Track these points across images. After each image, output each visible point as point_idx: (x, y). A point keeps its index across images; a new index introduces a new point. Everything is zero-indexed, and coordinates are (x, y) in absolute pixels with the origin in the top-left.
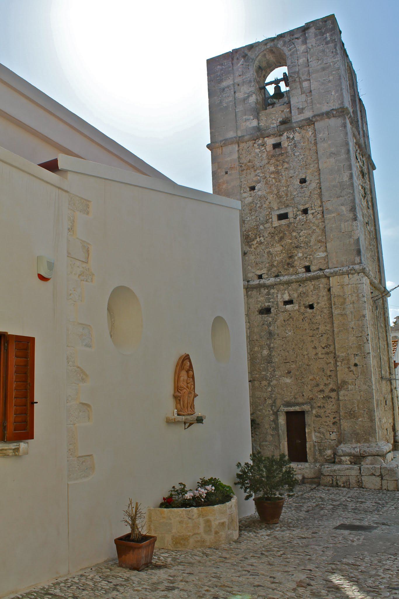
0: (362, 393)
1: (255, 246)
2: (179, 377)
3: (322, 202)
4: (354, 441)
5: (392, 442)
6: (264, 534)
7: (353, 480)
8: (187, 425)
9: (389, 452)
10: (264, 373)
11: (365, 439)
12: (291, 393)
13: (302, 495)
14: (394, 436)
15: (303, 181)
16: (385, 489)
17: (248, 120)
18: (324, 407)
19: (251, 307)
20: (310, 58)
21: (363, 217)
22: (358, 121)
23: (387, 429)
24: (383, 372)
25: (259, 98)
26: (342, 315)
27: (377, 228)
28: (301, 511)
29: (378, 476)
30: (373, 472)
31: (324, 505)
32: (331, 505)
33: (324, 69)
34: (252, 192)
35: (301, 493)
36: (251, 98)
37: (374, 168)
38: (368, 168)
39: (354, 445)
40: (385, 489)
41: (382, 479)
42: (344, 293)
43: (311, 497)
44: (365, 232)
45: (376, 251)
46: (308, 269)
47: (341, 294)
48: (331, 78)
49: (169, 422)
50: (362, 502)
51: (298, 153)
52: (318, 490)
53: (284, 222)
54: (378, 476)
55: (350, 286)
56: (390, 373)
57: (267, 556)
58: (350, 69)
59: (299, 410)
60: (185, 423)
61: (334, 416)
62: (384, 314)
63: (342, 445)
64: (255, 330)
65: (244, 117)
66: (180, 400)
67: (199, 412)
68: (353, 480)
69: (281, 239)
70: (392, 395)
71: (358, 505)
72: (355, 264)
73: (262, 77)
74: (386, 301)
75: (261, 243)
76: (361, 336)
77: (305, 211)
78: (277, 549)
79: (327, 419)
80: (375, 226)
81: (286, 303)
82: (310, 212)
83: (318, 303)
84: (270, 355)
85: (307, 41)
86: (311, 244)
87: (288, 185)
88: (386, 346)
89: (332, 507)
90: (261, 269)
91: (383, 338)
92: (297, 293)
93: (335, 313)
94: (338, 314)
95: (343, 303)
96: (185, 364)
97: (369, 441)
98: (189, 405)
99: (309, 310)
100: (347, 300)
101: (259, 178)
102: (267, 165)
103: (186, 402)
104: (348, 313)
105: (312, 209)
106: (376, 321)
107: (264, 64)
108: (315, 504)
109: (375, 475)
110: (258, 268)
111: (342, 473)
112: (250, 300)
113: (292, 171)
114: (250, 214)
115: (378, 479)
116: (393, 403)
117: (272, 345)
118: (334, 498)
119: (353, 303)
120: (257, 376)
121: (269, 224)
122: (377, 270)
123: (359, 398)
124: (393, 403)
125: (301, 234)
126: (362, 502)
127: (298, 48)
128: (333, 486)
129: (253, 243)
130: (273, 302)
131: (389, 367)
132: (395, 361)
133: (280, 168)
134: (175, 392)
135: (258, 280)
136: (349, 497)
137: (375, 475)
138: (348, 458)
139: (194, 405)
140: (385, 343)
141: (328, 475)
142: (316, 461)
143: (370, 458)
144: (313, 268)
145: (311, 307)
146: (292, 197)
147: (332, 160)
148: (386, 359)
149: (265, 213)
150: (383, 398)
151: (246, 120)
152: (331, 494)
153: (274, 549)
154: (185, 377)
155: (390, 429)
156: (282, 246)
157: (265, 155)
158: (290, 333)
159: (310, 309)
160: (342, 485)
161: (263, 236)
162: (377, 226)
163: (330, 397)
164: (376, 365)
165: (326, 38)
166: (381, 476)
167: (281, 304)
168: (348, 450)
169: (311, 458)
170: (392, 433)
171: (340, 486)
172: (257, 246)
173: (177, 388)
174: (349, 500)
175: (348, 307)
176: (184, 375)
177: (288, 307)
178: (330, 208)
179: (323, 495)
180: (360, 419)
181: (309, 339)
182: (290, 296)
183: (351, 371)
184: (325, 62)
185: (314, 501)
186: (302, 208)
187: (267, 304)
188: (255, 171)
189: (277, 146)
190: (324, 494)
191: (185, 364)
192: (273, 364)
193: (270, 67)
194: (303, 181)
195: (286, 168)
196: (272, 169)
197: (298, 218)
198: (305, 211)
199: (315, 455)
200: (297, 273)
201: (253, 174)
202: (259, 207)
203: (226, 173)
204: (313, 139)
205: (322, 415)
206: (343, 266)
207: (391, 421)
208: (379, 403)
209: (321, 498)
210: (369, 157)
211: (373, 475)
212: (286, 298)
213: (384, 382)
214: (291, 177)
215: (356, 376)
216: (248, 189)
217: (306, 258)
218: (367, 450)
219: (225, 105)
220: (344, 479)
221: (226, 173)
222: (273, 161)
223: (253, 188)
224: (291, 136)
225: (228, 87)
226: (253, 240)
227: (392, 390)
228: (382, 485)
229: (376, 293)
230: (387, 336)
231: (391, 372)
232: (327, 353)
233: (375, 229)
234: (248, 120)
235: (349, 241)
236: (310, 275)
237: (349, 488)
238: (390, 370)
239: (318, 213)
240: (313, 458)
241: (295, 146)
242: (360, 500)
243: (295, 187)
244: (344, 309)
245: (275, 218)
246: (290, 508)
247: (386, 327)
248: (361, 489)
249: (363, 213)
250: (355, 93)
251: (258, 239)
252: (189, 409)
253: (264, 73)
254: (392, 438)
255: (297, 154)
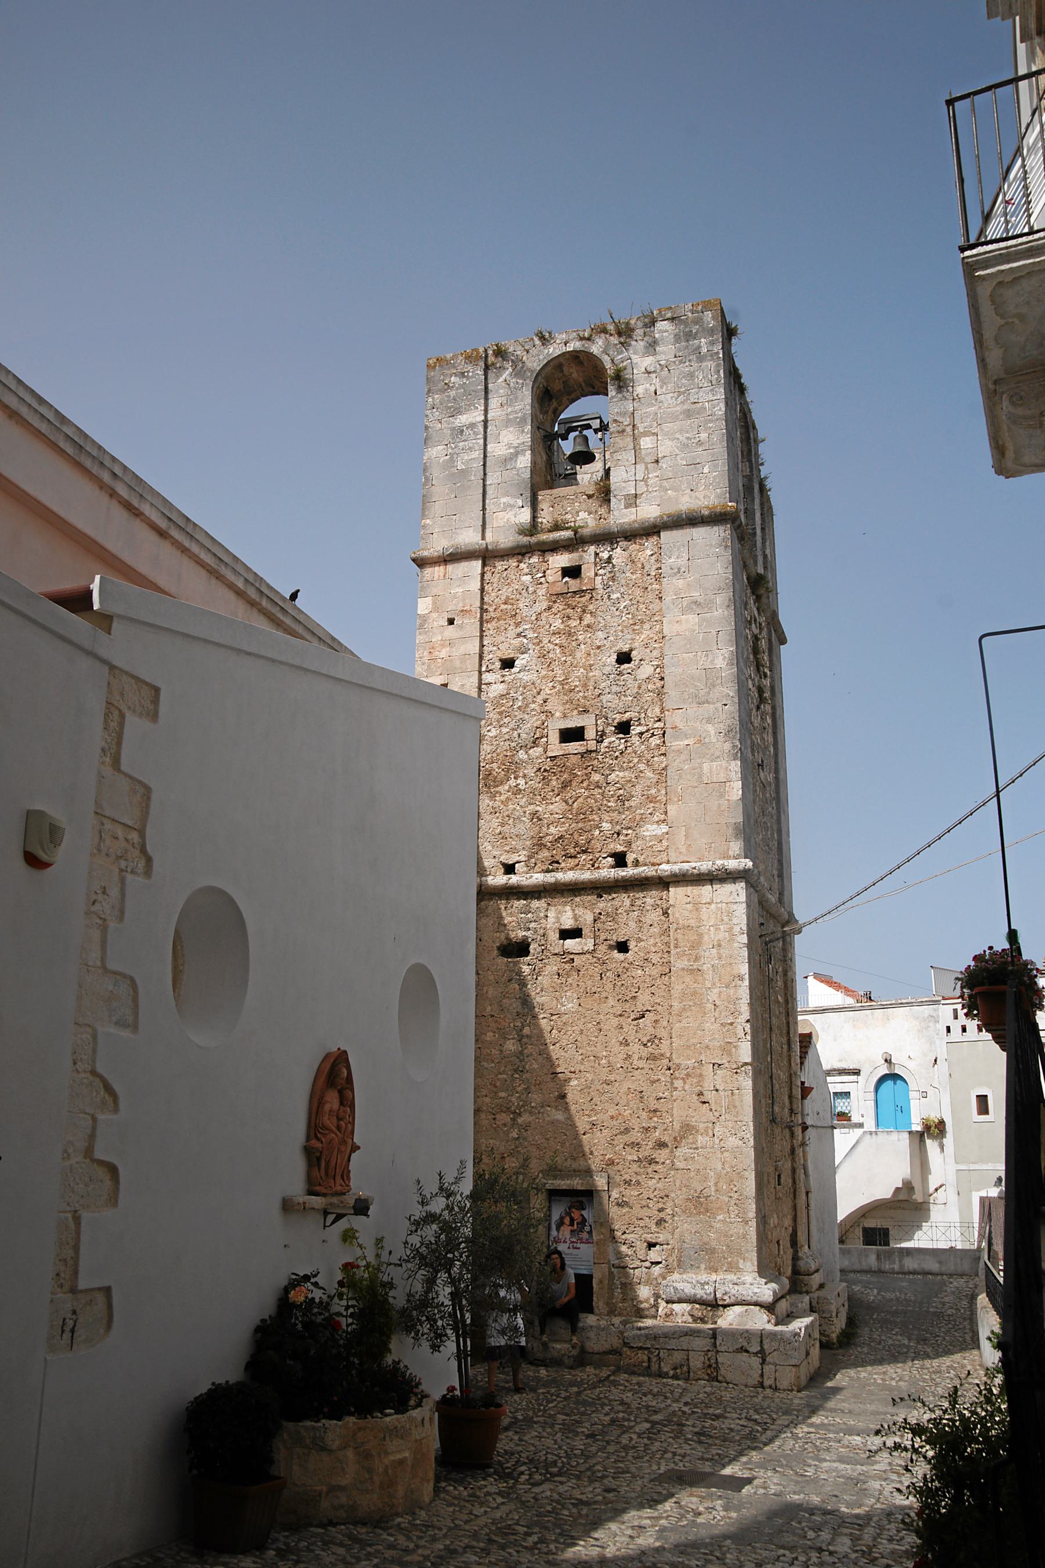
0: (726, 1154)
1: (503, 798)
2: (321, 1103)
3: (662, 711)
4: (703, 1266)
5: (789, 1272)
6: (493, 1489)
7: (697, 1362)
8: (331, 1218)
9: (782, 1297)
10: (502, 1094)
11: (730, 1263)
12: (563, 1144)
13: (579, 1393)
14: (793, 1259)
15: (624, 658)
16: (770, 1387)
17: (512, 506)
18: (638, 1183)
19: (485, 937)
20: (662, 387)
21: (753, 751)
22: (755, 534)
23: (778, 1242)
24: (776, 1109)
25: (539, 461)
26: (691, 971)
27: (781, 777)
28: (577, 1434)
29: (756, 1354)
30: (745, 1344)
31: (629, 1420)
32: (647, 1421)
33: (688, 414)
34: (506, 672)
35: (575, 1389)
36: (521, 458)
37: (783, 641)
38: (770, 641)
39: (704, 1277)
40: (770, 1387)
41: (764, 1362)
42: (699, 920)
43: (600, 1399)
44: (754, 785)
45: (775, 827)
46: (620, 860)
47: (692, 923)
48: (704, 436)
49: (287, 1206)
50: (717, 1417)
51: (619, 595)
52: (615, 1384)
53: (574, 747)
54: (756, 1354)
55: (713, 906)
56: (791, 1111)
57: (503, 1547)
58: (746, 418)
59: (580, 1188)
60: (326, 1213)
61: (661, 1205)
62: (785, 973)
63: (676, 1276)
64: (490, 993)
65: (504, 500)
66: (319, 1159)
67: (359, 1186)
68: (697, 1362)
69: (565, 785)
70: (793, 1160)
71: (707, 1425)
72: (729, 858)
73: (550, 412)
74: (791, 944)
75: (517, 791)
76: (731, 1024)
77: (624, 728)
78: (525, 1529)
79: (645, 1212)
80: (777, 771)
81: (566, 934)
82: (635, 730)
83: (639, 940)
84: (521, 1052)
85: (657, 349)
86: (632, 804)
87: (591, 665)
88: (785, 1047)
89: (648, 1425)
90: (514, 850)
91: (779, 1028)
92: (592, 910)
93: (677, 965)
94: (683, 969)
95: (696, 945)
96: (334, 1076)
97: (739, 1270)
98: (339, 1172)
99: (616, 954)
100: (706, 938)
101: (525, 641)
102: (546, 614)
103: (333, 1163)
104: (705, 967)
105: (640, 724)
106: (766, 989)
107: (557, 386)
108: (607, 1418)
109: (747, 1351)
110: (507, 848)
111: (672, 1344)
112: (484, 921)
113: (600, 635)
114: (498, 721)
115: (756, 1361)
116: (794, 1182)
117: (526, 1030)
118: (654, 1403)
119: (719, 945)
120: (487, 1100)
121: (540, 750)
122: (775, 872)
123: (719, 1167)
124: (794, 1182)
125: (612, 777)
126: (717, 1417)
127: (635, 361)
128: (649, 1375)
129: (499, 789)
130: (535, 931)
131: (790, 1097)
132: (803, 1083)
133: (573, 623)
134: (308, 1139)
135: (506, 877)
136: (686, 1404)
137: (747, 1351)
138: (686, 1307)
139: (349, 1171)
140: (784, 1040)
141: (641, 1348)
142: (612, 1312)
143: (738, 1309)
144: (630, 858)
145: (623, 947)
146: (597, 692)
147: (692, 619)
148: (784, 1076)
149: (533, 722)
150: (772, 1168)
151: (508, 507)
152: (645, 1395)
153: (517, 1528)
154: (336, 1105)
155: (786, 1243)
156: (566, 802)
157: (542, 591)
158: (570, 1005)
159: (620, 952)
160: (671, 1373)
161: (525, 776)
162: (782, 773)
163: (652, 1161)
164: (762, 1091)
165: (699, 347)
166: (762, 1354)
167: (554, 936)
168: (688, 1290)
169: (601, 1304)
170: (790, 1251)
171: (665, 1375)
172: (508, 799)
173: (314, 1128)
174: (685, 1409)
175: (707, 954)
176: (332, 1100)
177: (570, 944)
178: (680, 725)
179: (628, 1396)
180: (721, 1217)
181: (615, 1021)
182: (575, 918)
183: (704, 1103)
184: (692, 400)
185: (607, 1408)
186: (618, 718)
187: (521, 934)
188: (517, 625)
189: (573, 572)
190: (629, 1394)
191: (334, 1076)
192: (525, 1076)
193: (569, 394)
194: (624, 658)
195: (588, 626)
196: (558, 624)
197: (606, 743)
198: (624, 728)
199: (611, 1296)
200: (594, 865)
201: (512, 632)
202: (519, 708)
203: (451, 622)
204: (654, 567)
205: (632, 1201)
206: (700, 860)
207: (788, 1222)
208: (765, 1179)
209: (622, 1403)
210: (774, 615)
211: (743, 1350)
212: (568, 923)
213: (777, 1131)
214: (599, 647)
215: (717, 1114)
216: (498, 664)
217: (618, 834)
218: (733, 1290)
219: (460, 466)
220: (678, 1357)
221: (451, 622)
222: (559, 606)
223: (508, 664)
224: (605, 555)
225: (472, 426)
226: (502, 783)
227: (793, 1151)
228: (762, 1375)
229: (771, 926)
230: (788, 1023)
231: (795, 1107)
232: (652, 1058)
233: (777, 779)
234: (512, 506)
235: (720, 806)
236: (624, 874)
237: (687, 1379)
238: (791, 1103)
239: (653, 735)
240: (607, 1304)
241: (613, 579)
242: (711, 1411)
243: (607, 670)
244: (697, 959)
245: (554, 737)
246: (552, 1426)
247: (787, 1002)
248: (715, 1383)
249: (752, 742)
250: (751, 471)
251: (512, 782)
252: (339, 1181)
253: (554, 404)
254: (790, 1262)
255: (614, 596)
